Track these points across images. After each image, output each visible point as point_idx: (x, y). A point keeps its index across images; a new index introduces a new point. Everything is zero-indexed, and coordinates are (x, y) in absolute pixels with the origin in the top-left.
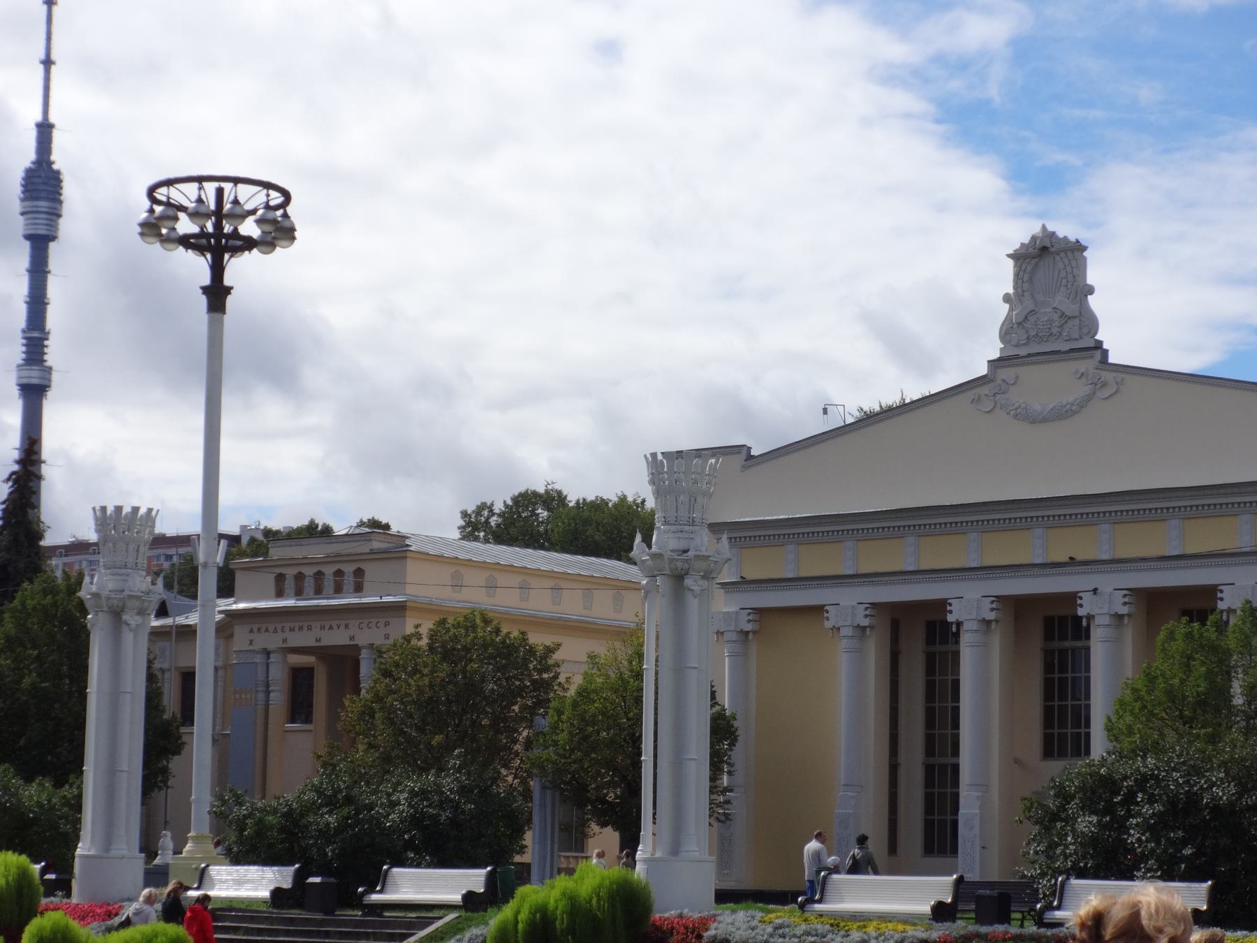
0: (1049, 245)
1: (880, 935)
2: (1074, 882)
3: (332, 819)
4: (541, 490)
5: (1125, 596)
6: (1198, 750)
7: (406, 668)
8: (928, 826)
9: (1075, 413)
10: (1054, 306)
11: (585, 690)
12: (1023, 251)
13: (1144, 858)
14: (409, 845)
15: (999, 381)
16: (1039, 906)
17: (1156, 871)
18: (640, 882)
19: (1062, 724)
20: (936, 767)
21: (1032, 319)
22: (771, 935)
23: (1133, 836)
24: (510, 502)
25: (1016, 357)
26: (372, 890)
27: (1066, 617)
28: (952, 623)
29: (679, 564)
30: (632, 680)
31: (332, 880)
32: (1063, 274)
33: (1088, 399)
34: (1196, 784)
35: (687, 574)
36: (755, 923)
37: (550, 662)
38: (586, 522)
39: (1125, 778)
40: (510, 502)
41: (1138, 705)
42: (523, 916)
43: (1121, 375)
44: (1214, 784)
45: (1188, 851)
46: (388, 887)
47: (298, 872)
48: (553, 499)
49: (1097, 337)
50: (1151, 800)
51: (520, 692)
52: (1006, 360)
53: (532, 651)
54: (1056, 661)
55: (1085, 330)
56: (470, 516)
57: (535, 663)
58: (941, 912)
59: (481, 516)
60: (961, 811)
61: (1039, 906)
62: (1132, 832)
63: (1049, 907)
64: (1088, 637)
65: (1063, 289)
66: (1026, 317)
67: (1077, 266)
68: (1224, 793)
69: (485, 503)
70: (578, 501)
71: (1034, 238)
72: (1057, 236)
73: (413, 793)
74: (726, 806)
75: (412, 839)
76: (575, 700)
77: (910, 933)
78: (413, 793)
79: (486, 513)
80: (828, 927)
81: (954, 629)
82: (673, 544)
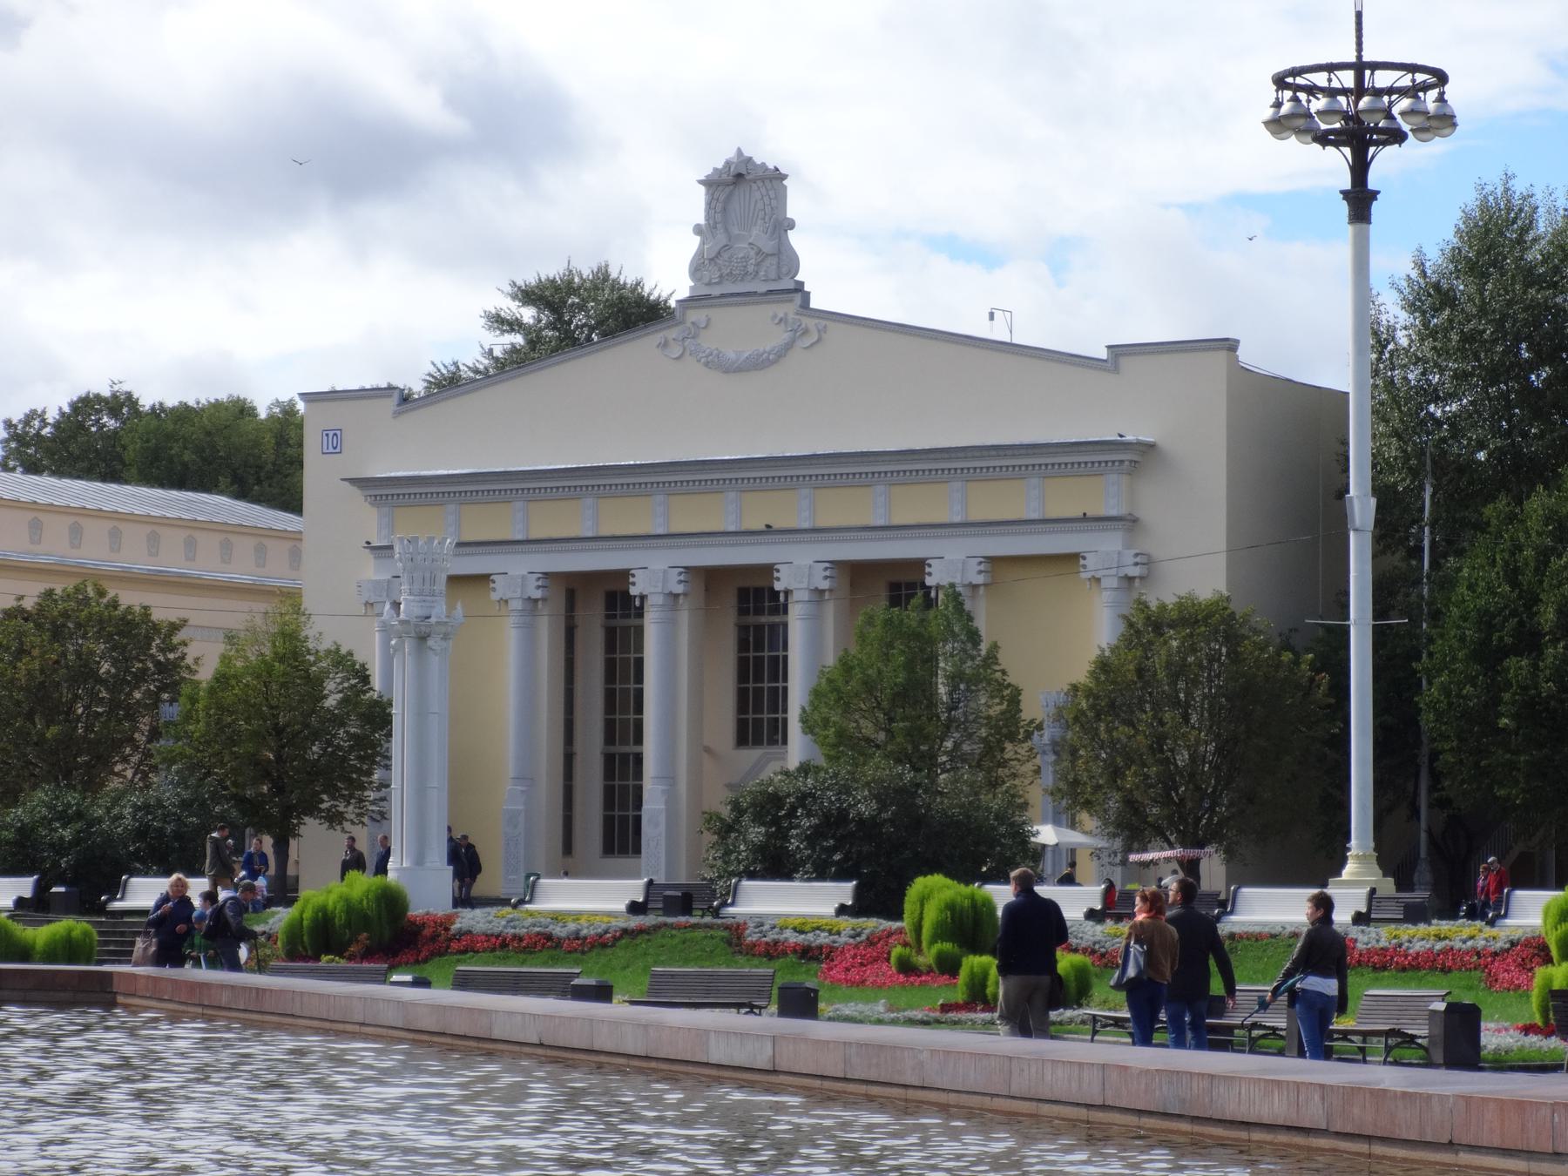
0: (744, 172)
1: (591, 925)
2: (745, 883)
3: (67, 834)
4: (106, 392)
5: (826, 569)
6: (848, 772)
7: (9, 648)
8: (608, 822)
9: (773, 363)
10: (750, 241)
11: (224, 676)
12: (716, 178)
13: (803, 862)
14: (135, 856)
15: (688, 324)
16: (715, 903)
17: (812, 873)
18: (393, 883)
19: (758, 709)
20: (617, 757)
21: (726, 256)
22: (505, 927)
23: (794, 844)
24: (67, 409)
25: (708, 297)
26: (113, 899)
27: (763, 589)
28: (635, 596)
29: (423, 629)
30: (277, 664)
31: (74, 889)
32: (760, 205)
33: (789, 346)
34: (845, 800)
35: (429, 636)
36: (491, 918)
37: (176, 640)
38: (170, 437)
39: (789, 795)
40: (67, 409)
41: (833, 697)
42: (308, 915)
43: (824, 322)
44: (859, 801)
45: (837, 857)
46: (129, 894)
47: (38, 882)
48: (122, 404)
49: (797, 278)
50: (809, 815)
51: (141, 676)
52: (696, 300)
53: (156, 628)
54: (751, 639)
55: (784, 270)
56: (15, 426)
57: (158, 641)
58: (635, 908)
59: (31, 427)
60: (645, 807)
61: (715, 903)
62: (792, 841)
63: (724, 904)
64: (786, 612)
65: (759, 222)
66: (719, 253)
67: (776, 198)
68: (866, 809)
69: (35, 410)
70: (154, 405)
71: (728, 163)
72: (754, 163)
73: (136, 808)
74: (381, 804)
75: (138, 850)
76: (212, 687)
77: (614, 924)
78: (136, 808)
79: (36, 423)
80: (549, 920)
81: (637, 603)
82: (418, 611)
